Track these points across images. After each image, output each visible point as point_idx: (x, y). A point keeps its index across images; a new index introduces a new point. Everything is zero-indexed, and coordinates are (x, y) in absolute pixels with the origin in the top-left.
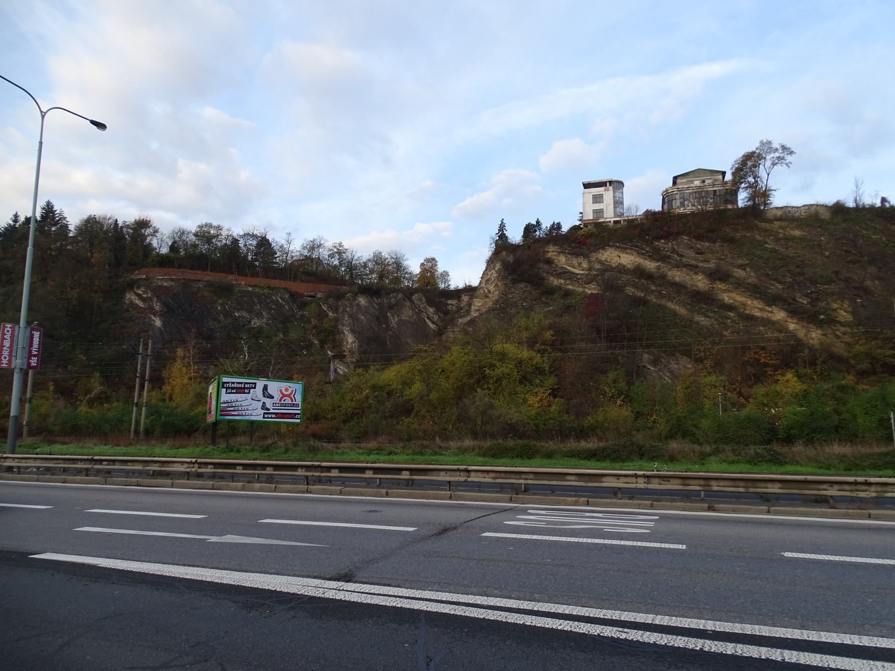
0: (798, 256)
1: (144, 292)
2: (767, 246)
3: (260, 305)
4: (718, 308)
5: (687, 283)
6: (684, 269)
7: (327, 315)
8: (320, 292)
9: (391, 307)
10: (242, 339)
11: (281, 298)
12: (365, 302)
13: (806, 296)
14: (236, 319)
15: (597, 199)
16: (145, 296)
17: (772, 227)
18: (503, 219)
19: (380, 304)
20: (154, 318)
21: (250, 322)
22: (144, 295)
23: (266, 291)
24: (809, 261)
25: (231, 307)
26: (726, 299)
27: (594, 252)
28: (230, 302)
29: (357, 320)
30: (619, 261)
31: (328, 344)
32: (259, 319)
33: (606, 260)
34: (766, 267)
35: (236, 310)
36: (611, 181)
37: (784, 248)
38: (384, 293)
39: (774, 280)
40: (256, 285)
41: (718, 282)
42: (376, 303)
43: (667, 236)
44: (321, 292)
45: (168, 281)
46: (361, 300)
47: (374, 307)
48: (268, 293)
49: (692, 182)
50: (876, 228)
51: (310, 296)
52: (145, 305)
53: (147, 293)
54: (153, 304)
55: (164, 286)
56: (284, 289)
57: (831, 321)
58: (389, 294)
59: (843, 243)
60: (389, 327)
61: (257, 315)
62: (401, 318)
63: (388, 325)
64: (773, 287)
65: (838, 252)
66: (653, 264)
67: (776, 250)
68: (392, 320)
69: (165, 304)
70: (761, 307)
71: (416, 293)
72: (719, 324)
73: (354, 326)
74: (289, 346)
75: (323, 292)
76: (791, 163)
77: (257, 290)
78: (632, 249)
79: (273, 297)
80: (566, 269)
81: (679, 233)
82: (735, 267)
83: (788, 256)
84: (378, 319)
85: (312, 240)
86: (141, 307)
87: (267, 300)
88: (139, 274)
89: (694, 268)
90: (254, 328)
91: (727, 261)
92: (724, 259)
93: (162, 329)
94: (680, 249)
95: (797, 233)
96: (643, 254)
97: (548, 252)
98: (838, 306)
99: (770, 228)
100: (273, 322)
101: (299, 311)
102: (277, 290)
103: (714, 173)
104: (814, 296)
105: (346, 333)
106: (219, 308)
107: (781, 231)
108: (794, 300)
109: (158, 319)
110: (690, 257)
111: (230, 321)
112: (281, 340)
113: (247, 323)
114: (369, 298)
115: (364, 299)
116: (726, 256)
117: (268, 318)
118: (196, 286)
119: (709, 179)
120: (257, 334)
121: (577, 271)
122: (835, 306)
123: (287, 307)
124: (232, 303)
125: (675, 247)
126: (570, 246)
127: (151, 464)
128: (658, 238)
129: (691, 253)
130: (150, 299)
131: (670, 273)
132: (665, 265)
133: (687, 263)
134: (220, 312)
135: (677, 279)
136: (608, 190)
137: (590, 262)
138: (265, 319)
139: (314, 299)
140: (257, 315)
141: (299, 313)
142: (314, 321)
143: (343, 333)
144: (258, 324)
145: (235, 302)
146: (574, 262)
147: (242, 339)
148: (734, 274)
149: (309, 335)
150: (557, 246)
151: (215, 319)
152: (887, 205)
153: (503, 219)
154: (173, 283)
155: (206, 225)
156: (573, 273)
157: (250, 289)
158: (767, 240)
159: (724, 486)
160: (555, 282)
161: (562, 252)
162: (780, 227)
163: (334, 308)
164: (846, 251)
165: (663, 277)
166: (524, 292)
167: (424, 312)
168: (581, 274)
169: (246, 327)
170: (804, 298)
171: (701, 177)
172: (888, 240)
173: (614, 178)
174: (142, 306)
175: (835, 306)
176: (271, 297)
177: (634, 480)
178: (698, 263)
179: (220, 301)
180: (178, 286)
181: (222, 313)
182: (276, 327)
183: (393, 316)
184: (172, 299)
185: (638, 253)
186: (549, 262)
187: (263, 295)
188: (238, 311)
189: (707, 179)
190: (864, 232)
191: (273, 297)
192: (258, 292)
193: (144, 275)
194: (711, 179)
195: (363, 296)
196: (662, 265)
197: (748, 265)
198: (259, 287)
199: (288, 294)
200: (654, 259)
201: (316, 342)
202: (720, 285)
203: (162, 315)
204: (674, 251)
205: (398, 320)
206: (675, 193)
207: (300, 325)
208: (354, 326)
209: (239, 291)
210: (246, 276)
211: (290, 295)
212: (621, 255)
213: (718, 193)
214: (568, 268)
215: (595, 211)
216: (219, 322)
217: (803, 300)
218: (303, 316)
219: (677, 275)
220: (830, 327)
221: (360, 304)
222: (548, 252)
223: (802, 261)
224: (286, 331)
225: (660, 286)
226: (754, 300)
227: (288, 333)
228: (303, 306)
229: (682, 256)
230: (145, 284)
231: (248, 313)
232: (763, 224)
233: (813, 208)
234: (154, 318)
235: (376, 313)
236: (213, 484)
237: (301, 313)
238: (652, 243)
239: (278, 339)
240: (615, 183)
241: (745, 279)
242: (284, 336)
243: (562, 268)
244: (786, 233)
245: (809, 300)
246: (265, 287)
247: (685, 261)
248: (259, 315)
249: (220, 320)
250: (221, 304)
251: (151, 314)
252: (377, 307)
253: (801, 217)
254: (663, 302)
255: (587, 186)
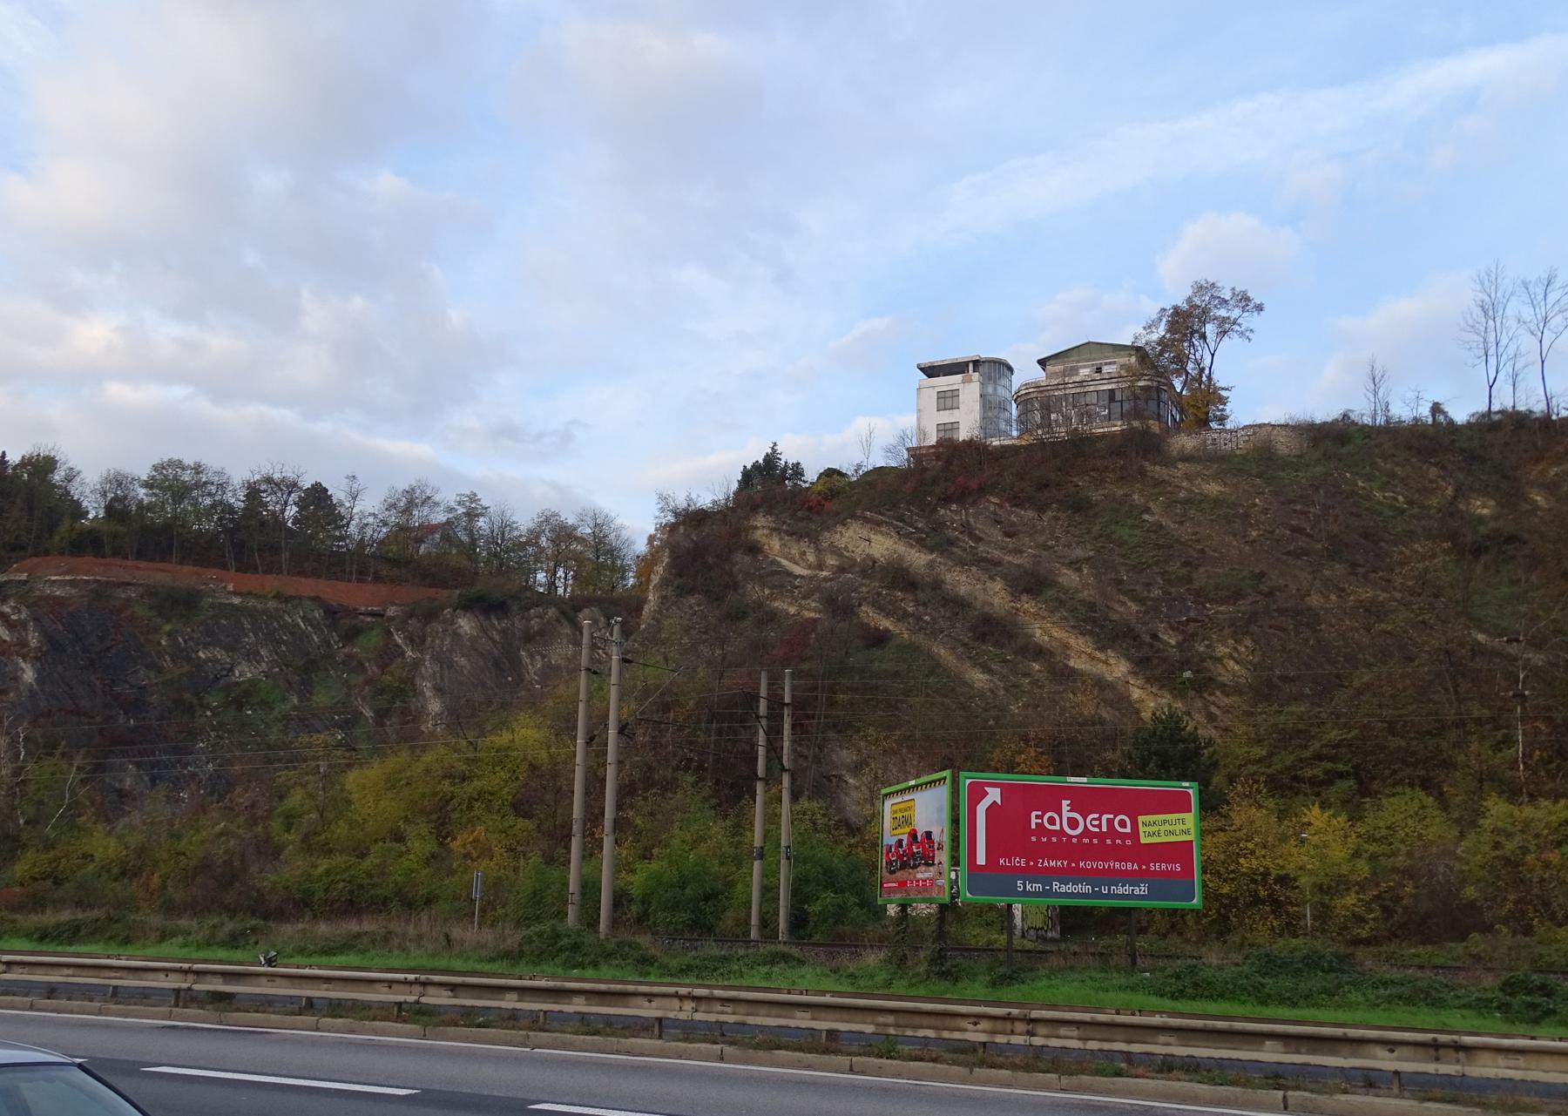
0: (1198, 541)
1: (17, 610)
2: (1146, 517)
3: (256, 635)
4: (1015, 653)
5: (976, 598)
6: (974, 569)
7: (403, 654)
8: (393, 604)
9: (529, 638)
10: (208, 707)
11: (303, 619)
12: (471, 627)
13: (1174, 629)
14: (200, 664)
15: (947, 400)
16: (14, 617)
17: (1170, 476)
18: (775, 444)
19: (504, 632)
20: (23, 665)
21: (231, 670)
22: (13, 617)
23: (272, 604)
24: (1215, 551)
25: (191, 639)
26: (1038, 632)
27: (828, 529)
28: (189, 630)
29: (451, 665)
30: (867, 550)
31: (393, 719)
32: (252, 665)
33: (846, 548)
34: (1122, 564)
35: (200, 647)
36: (978, 361)
37: (1175, 522)
38: (515, 608)
39: (1125, 593)
40: (249, 593)
41: (1024, 598)
42: (496, 630)
43: (962, 496)
44: (396, 604)
45: (65, 585)
46: (462, 624)
47: (492, 639)
48: (277, 609)
49: (1074, 371)
50: (1393, 475)
51: (373, 614)
52: (12, 638)
53: (19, 612)
54: (27, 634)
55: (56, 597)
56: (311, 599)
57: (1204, 684)
58: (528, 609)
59: (1295, 511)
60: (522, 680)
61: (248, 655)
62: (550, 661)
63: (520, 679)
64: (1121, 609)
65: (1277, 531)
66: (923, 556)
67: (1161, 525)
68: (530, 667)
69: (48, 637)
70: (1089, 650)
71: (586, 607)
72: (1006, 689)
73: (442, 679)
74: (306, 722)
75: (400, 606)
76: (1251, 331)
77: (252, 602)
78: (891, 524)
79: (287, 618)
80: (779, 565)
81: (982, 491)
82: (1063, 564)
83: (1178, 541)
84: (497, 665)
85: (407, 489)
86: (5, 641)
87: (272, 624)
88: (18, 570)
89: (989, 566)
90: (238, 684)
91: (1055, 552)
92: (1051, 547)
93: (35, 687)
94: (978, 526)
95: (1213, 489)
96: (908, 535)
97: (756, 528)
98: (1227, 650)
99: (1167, 478)
100: (281, 670)
101: (343, 646)
102: (296, 602)
103: (1120, 350)
104: (1191, 628)
105: (428, 694)
106: (164, 643)
107: (1184, 484)
108: (1155, 636)
109: (29, 666)
110: (993, 543)
111: (184, 670)
112: (295, 708)
113: (225, 673)
114: (481, 618)
115: (469, 620)
116: (1057, 539)
117: (271, 662)
118: (123, 596)
119: (1110, 363)
120: (242, 697)
121: (798, 570)
122: (1221, 650)
123: (315, 638)
124: (193, 631)
125: (971, 520)
126: (793, 515)
127: (209, 978)
128: (946, 500)
129: (996, 534)
130: (23, 624)
131: (949, 577)
132: (942, 560)
133: (984, 555)
134: (164, 650)
135: (962, 590)
136: (971, 381)
137: (818, 550)
138: (264, 665)
139: (379, 619)
140: (248, 655)
141: (343, 650)
142: (372, 669)
143: (422, 693)
144: (249, 675)
145: (201, 628)
146: (793, 552)
147: (208, 707)
148: (1060, 580)
149: (356, 699)
150: (771, 515)
151: (151, 666)
152: (1441, 418)
153: (775, 444)
154: (73, 591)
155: (171, 463)
156: (790, 574)
157: (236, 601)
158: (1151, 505)
159: (68, 976)
160: (755, 592)
161: (775, 529)
162: (1187, 477)
163: (417, 640)
164: (1295, 530)
165: (937, 585)
166: (695, 613)
167: (600, 648)
168: (802, 577)
169: (222, 682)
170: (1171, 632)
171: (1094, 360)
172: (1411, 503)
173: (985, 354)
174: (8, 638)
175: (1221, 650)
176: (281, 617)
177: (676, 1003)
178: (1005, 554)
179: (168, 628)
180: (83, 596)
181: (167, 653)
182: (287, 680)
183: (532, 656)
184: (63, 625)
185: (898, 533)
186: (754, 549)
187: (265, 612)
188: (206, 646)
189: (1106, 364)
190: (1360, 484)
191: (287, 618)
192: (254, 607)
193: (24, 572)
194: (1114, 363)
195: (468, 615)
196: (938, 560)
197: (1088, 559)
198: (257, 596)
199: (321, 611)
200: (925, 547)
201: (368, 713)
202: (1028, 605)
203: (38, 659)
204: (967, 528)
205: (543, 666)
206: (1032, 396)
207: (340, 677)
208: (442, 679)
209: (212, 606)
210: (255, 570)
211: (325, 612)
212: (873, 536)
213: (1118, 396)
214: (784, 562)
215: (942, 427)
216: (160, 671)
217: (1170, 637)
218: (350, 656)
219: (961, 582)
220: (1201, 697)
221: (461, 631)
222: (756, 528)
223: (1202, 551)
224: (306, 689)
225: (925, 604)
226: (1079, 637)
227: (311, 693)
228: (352, 635)
229: (979, 540)
230: (16, 593)
231: (227, 652)
232: (1158, 468)
233: (1263, 432)
234: (23, 665)
235: (495, 651)
236: (100, 1007)
237: (346, 650)
238: (934, 511)
239: (285, 707)
240: (987, 365)
241: (1077, 591)
242: (300, 701)
243: (774, 562)
244: (1194, 489)
245: (1180, 638)
246: (270, 595)
247: (982, 551)
248: (253, 656)
249: (164, 668)
250: (169, 635)
251: (18, 656)
252: (497, 638)
253: (1238, 452)
254: (920, 639)
255: (931, 371)
